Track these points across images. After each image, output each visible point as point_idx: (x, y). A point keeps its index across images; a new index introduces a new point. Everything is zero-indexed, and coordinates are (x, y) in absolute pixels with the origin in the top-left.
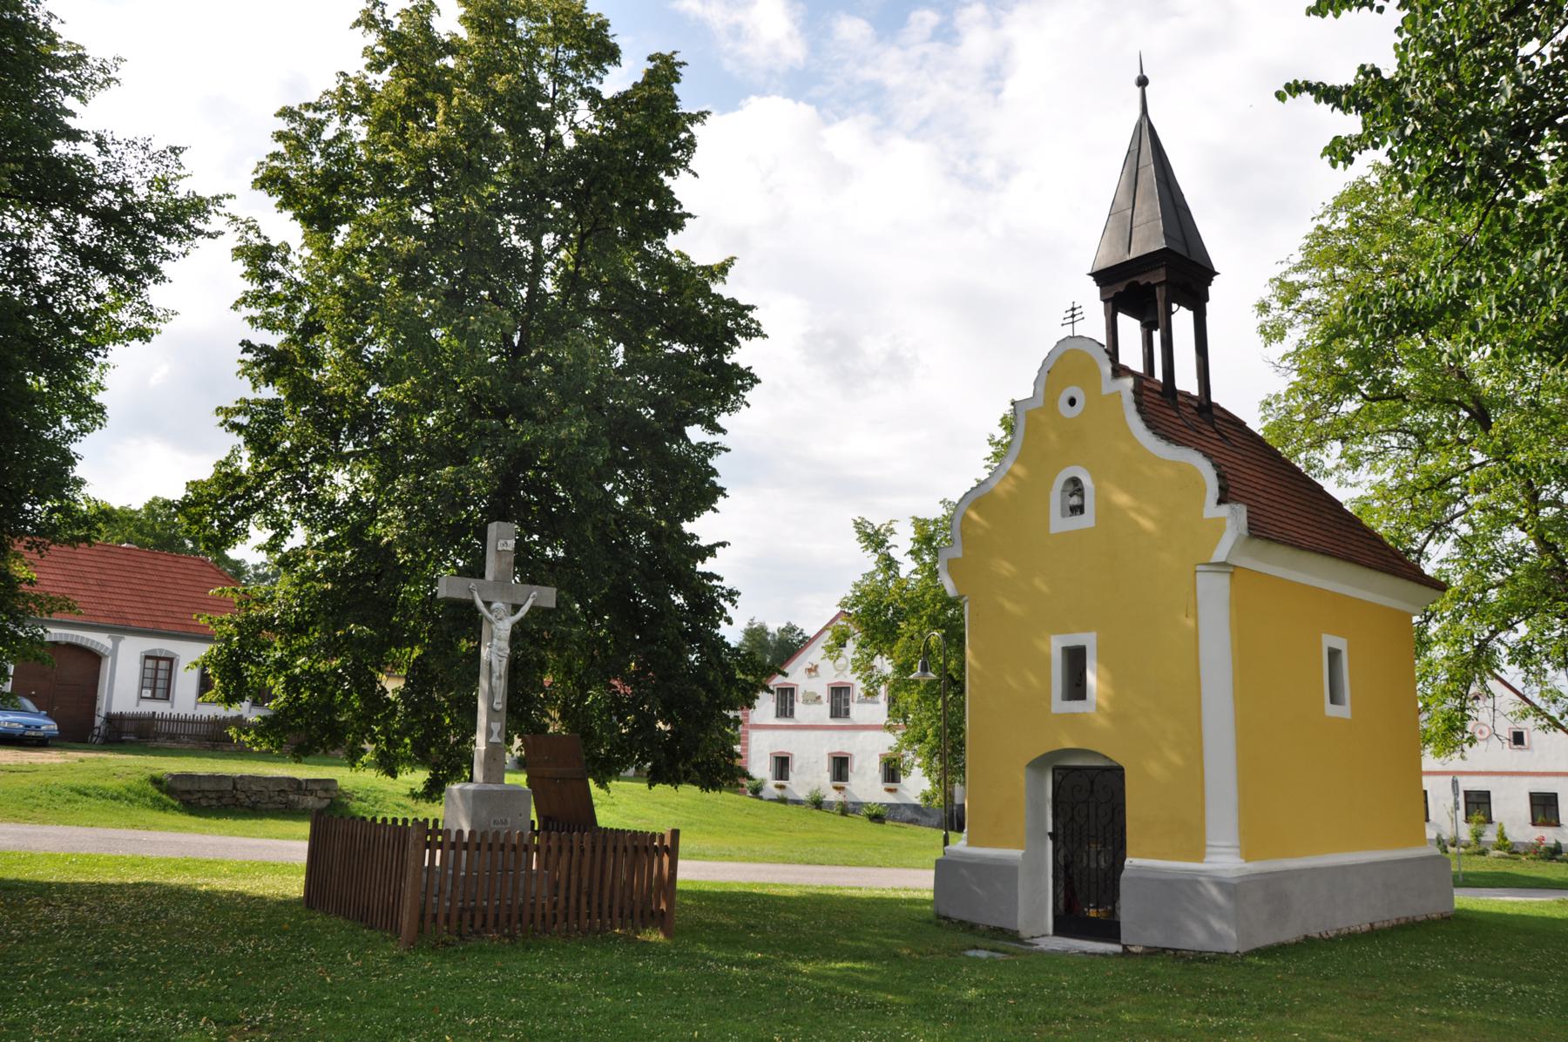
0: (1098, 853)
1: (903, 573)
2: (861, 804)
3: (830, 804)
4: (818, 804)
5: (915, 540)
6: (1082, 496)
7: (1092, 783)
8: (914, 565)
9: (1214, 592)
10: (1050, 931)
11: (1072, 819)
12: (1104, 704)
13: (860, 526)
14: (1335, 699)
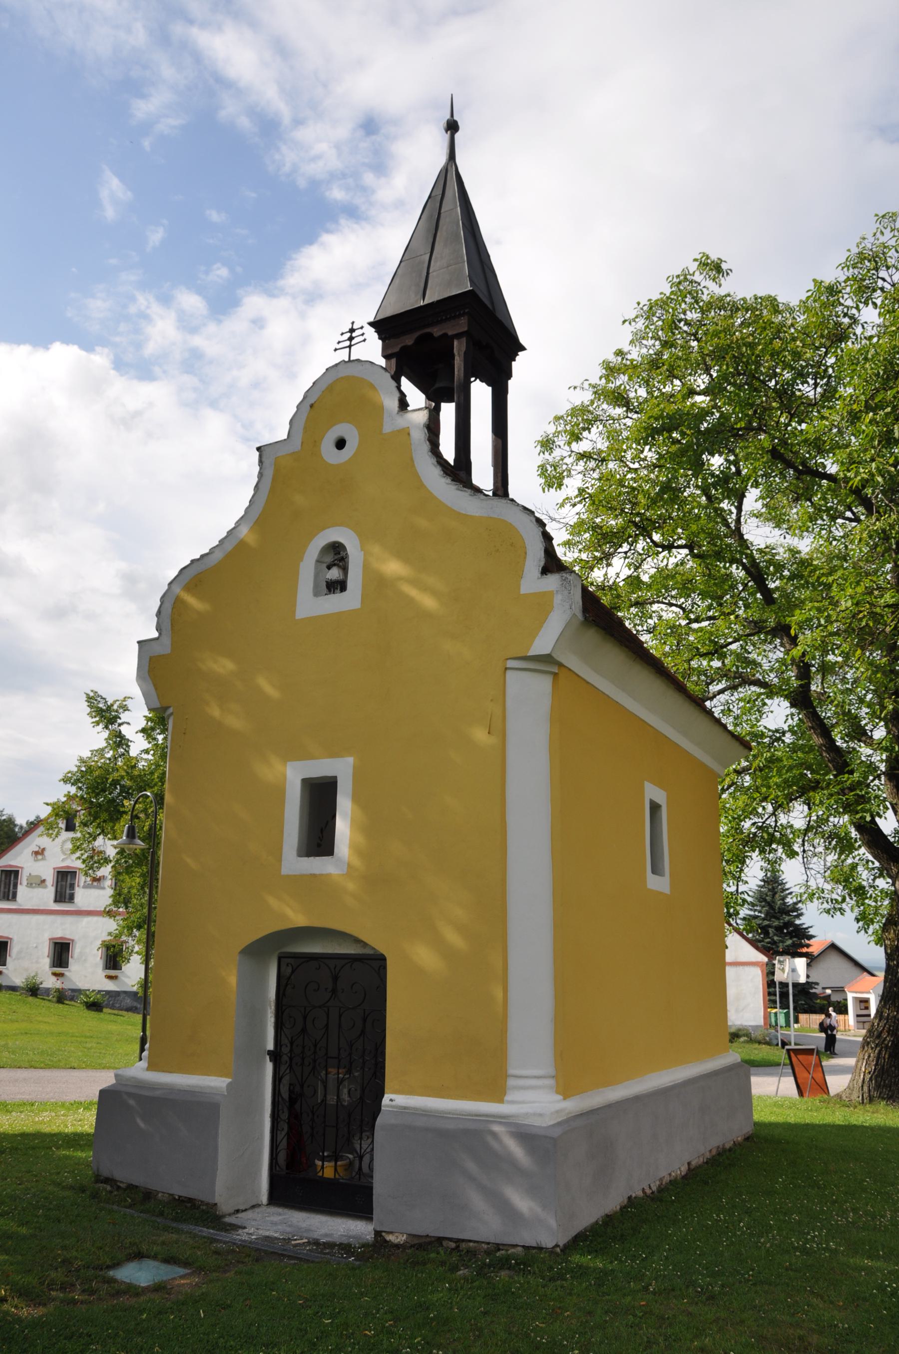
0: (340, 1082)
1: (134, 752)
2: (79, 991)
3: (47, 991)
4: (34, 990)
5: (148, 719)
6: (345, 569)
7: (335, 978)
8: (146, 745)
9: (529, 699)
10: (264, 1199)
11: (304, 1031)
12: (357, 862)
13: (92, 699)
14: (656, 870)
